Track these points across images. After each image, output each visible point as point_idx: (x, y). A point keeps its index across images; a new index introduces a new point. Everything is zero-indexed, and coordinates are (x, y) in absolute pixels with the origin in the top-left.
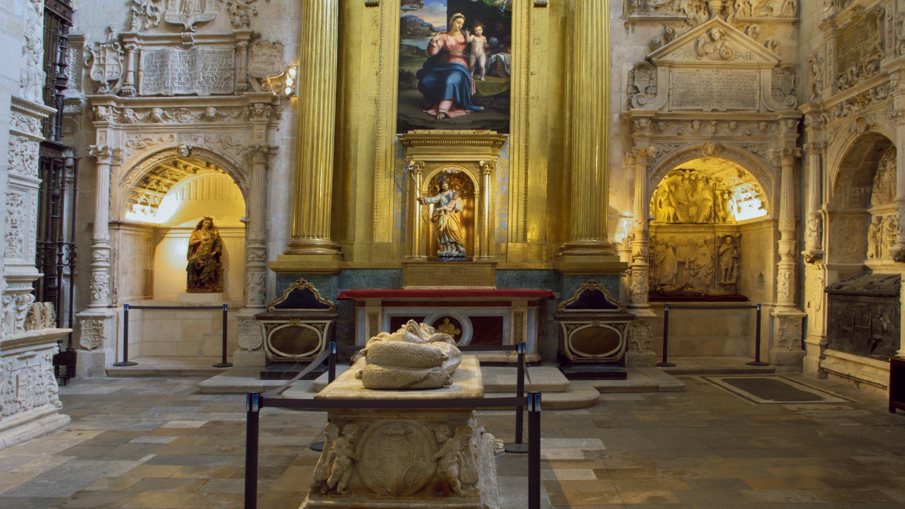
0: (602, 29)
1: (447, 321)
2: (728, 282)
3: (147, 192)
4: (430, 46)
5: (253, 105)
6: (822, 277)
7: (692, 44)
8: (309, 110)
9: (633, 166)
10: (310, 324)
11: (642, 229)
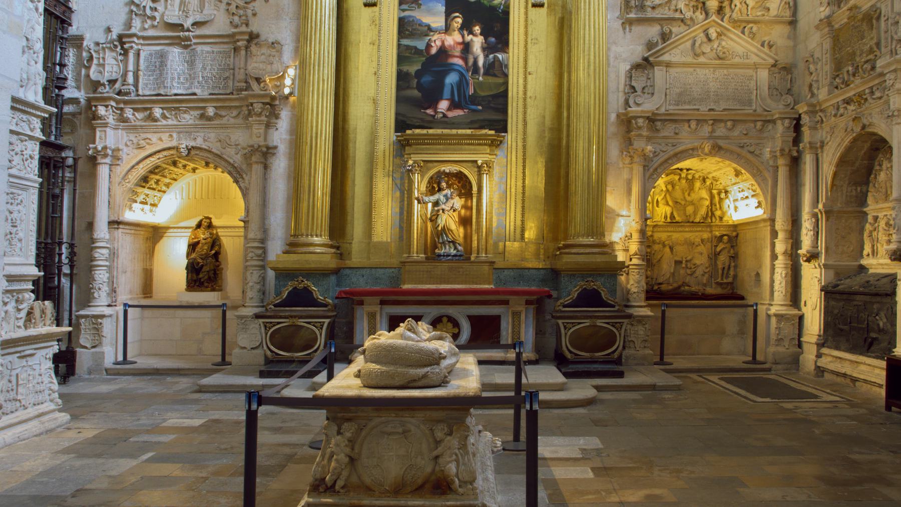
0: (599, 29)
1: (445, 320)
2: (725, 281)
3: (146, 191)
4: (429, 46)
5: (252, 104)
6: (819, 276)
7: (689, 44)
8: (308, 110)
9: (630, 166)
10: (309, 323)
11: (639, 228)
